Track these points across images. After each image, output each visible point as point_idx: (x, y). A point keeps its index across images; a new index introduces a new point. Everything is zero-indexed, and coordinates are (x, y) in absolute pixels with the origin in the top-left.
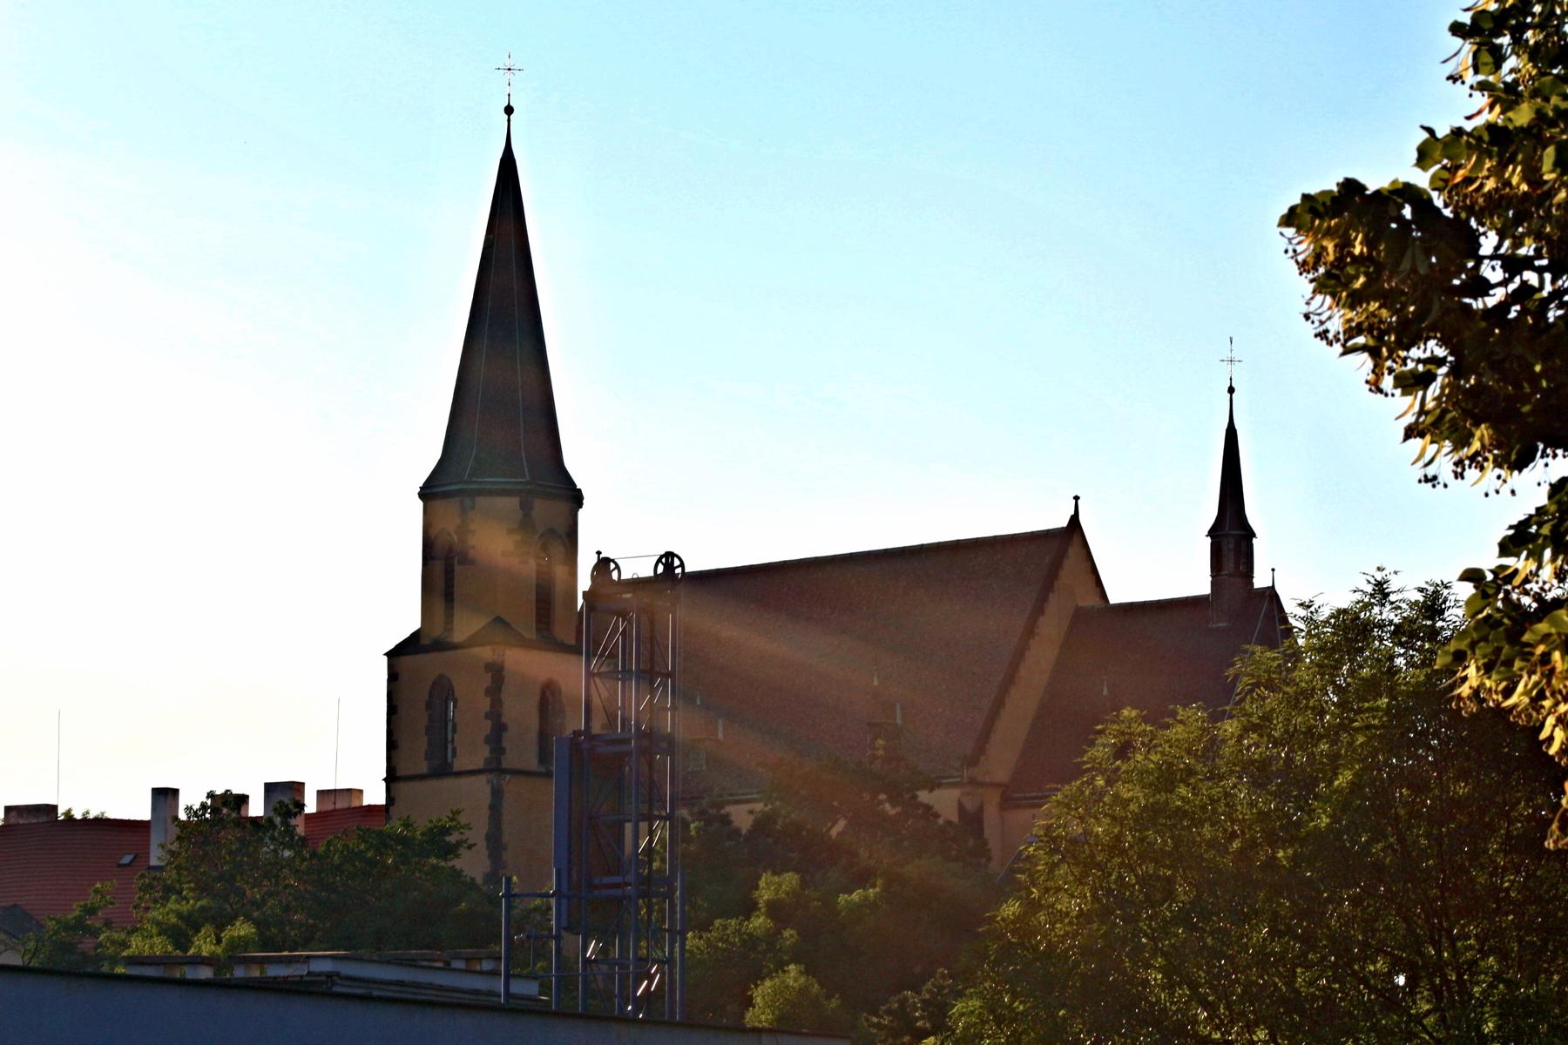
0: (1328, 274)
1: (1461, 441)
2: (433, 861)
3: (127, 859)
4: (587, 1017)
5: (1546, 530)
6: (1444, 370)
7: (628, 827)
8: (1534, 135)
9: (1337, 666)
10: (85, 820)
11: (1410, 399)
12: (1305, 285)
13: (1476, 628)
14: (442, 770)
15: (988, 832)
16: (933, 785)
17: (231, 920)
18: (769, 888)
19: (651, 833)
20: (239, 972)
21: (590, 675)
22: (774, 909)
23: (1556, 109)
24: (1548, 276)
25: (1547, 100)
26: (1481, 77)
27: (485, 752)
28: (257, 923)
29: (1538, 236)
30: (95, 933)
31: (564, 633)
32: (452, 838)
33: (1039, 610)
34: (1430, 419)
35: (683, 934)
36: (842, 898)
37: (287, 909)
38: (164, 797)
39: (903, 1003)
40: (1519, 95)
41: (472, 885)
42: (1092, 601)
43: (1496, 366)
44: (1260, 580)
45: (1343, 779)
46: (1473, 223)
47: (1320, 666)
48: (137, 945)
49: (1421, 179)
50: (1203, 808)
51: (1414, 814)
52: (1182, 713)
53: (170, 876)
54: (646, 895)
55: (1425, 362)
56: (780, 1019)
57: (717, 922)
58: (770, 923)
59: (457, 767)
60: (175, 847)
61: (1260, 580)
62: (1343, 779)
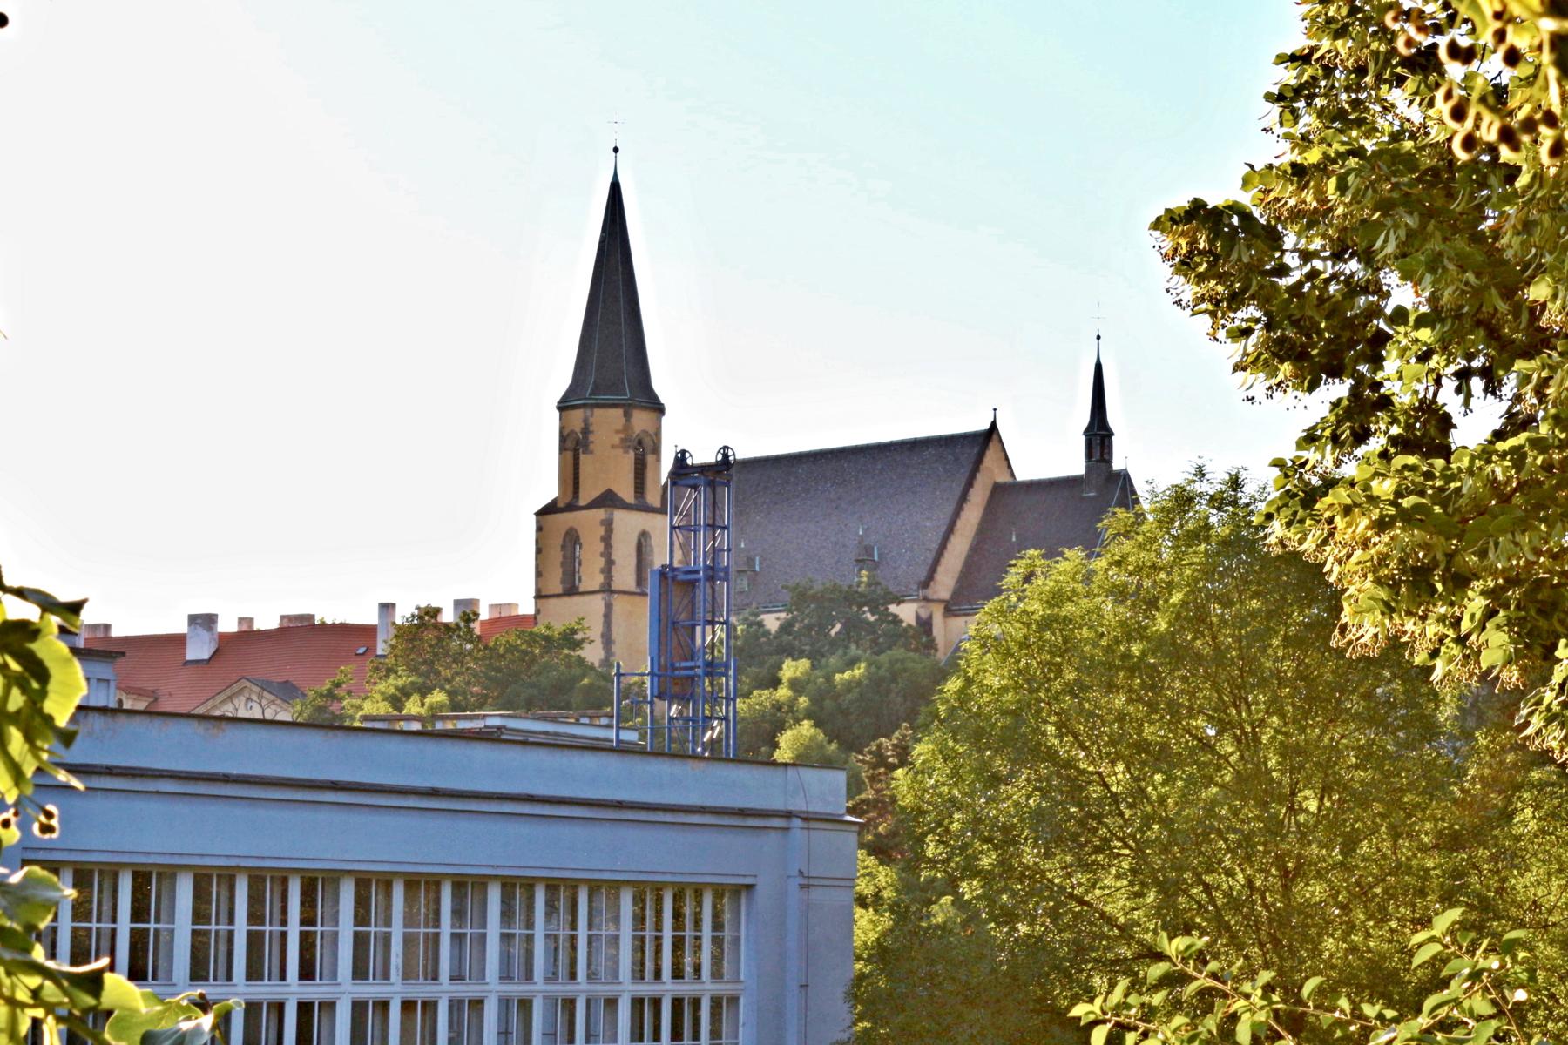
0: (1182, 262)
1: (1273, 373)
2: (566, 651)
3: (361, 651)
4: (673, 756)
5: (1327, 433)
6: (1260, 326)
7: (698, 629)
8: (1322, 168)
9: (1172, 521)
10: (334, 625)
11: (1236, 345)
12: (1166, 269)
13: (1281, 497)
14: (571, 590)
15: (935, 632)
16: (899, 602)
17: (430, 690)
18: (792, 669)
19: (714, 633)
20: (439, 726)
21: (673, 528)
22: (795, 685)
23: (1337, 152)
24: (1329, 263)
25: (1330, 145)
26: (1285, 130)
27: (600, 579)
28: (449, 693)
29: (1324, 236)
30: (340, 700)
31: (653, 498)
32: (578, 637)
33: (970, 484)
34: (1250, 359)
35: (734, 700)
36: (838, 677)
37: (468, 683)
38: (387, 608)
39: (879, 746)
40: (1310, 142)
41: (592, 668)
42: (1008, 479)
43: (1295, 323)
44: (1117, 465)
45: (1176, 598)
46: (1280, 228)
47: (1160, 521)
48: (369, 708)
49: (1246, 199)
50: (1082, 617)
51: (1223, 622)
52: (1068, 553)
53: (391, 661)
54: (707, 674)
55: (1247, 321)
56: (798, 756)
57: (756, 692)
58: (790, 693)
59: (581, 589)
60: (394, 642)
61: (1117, 465)
62: (1176, 598)
